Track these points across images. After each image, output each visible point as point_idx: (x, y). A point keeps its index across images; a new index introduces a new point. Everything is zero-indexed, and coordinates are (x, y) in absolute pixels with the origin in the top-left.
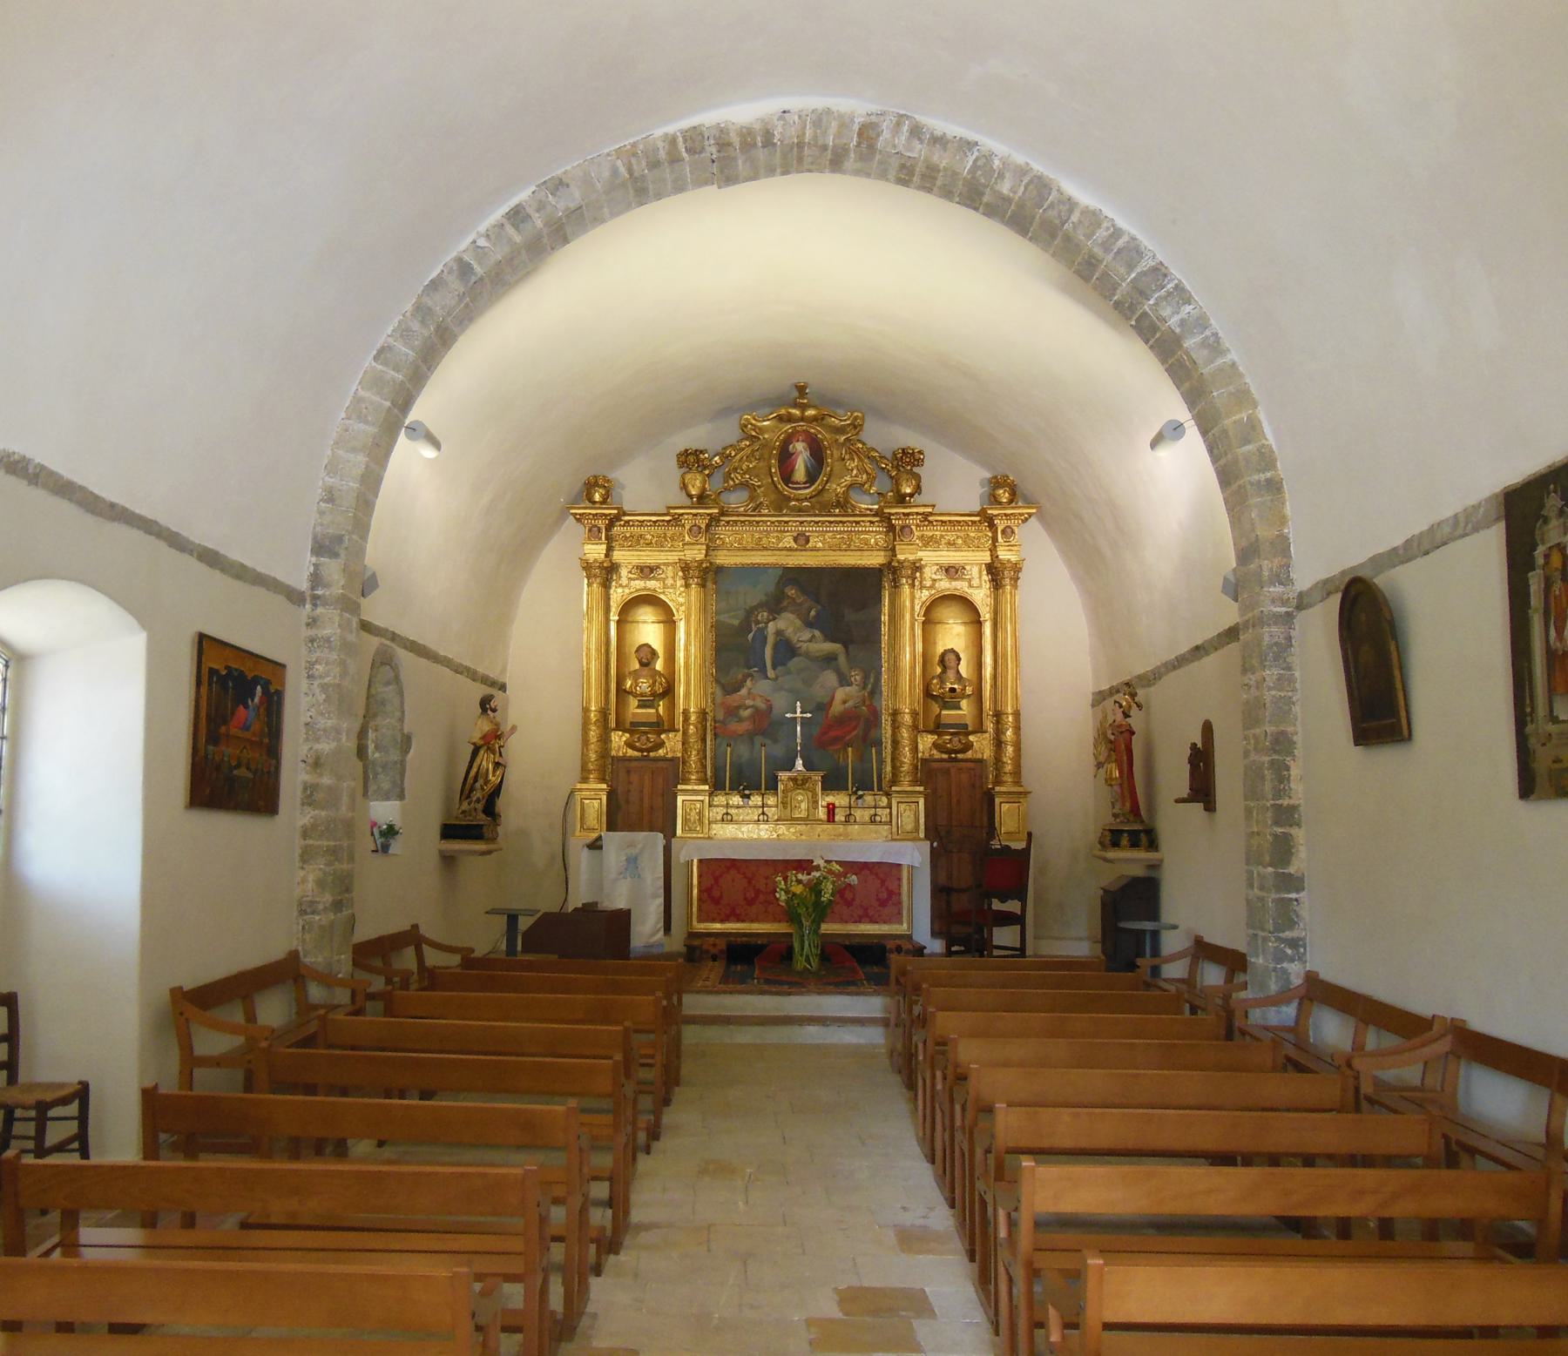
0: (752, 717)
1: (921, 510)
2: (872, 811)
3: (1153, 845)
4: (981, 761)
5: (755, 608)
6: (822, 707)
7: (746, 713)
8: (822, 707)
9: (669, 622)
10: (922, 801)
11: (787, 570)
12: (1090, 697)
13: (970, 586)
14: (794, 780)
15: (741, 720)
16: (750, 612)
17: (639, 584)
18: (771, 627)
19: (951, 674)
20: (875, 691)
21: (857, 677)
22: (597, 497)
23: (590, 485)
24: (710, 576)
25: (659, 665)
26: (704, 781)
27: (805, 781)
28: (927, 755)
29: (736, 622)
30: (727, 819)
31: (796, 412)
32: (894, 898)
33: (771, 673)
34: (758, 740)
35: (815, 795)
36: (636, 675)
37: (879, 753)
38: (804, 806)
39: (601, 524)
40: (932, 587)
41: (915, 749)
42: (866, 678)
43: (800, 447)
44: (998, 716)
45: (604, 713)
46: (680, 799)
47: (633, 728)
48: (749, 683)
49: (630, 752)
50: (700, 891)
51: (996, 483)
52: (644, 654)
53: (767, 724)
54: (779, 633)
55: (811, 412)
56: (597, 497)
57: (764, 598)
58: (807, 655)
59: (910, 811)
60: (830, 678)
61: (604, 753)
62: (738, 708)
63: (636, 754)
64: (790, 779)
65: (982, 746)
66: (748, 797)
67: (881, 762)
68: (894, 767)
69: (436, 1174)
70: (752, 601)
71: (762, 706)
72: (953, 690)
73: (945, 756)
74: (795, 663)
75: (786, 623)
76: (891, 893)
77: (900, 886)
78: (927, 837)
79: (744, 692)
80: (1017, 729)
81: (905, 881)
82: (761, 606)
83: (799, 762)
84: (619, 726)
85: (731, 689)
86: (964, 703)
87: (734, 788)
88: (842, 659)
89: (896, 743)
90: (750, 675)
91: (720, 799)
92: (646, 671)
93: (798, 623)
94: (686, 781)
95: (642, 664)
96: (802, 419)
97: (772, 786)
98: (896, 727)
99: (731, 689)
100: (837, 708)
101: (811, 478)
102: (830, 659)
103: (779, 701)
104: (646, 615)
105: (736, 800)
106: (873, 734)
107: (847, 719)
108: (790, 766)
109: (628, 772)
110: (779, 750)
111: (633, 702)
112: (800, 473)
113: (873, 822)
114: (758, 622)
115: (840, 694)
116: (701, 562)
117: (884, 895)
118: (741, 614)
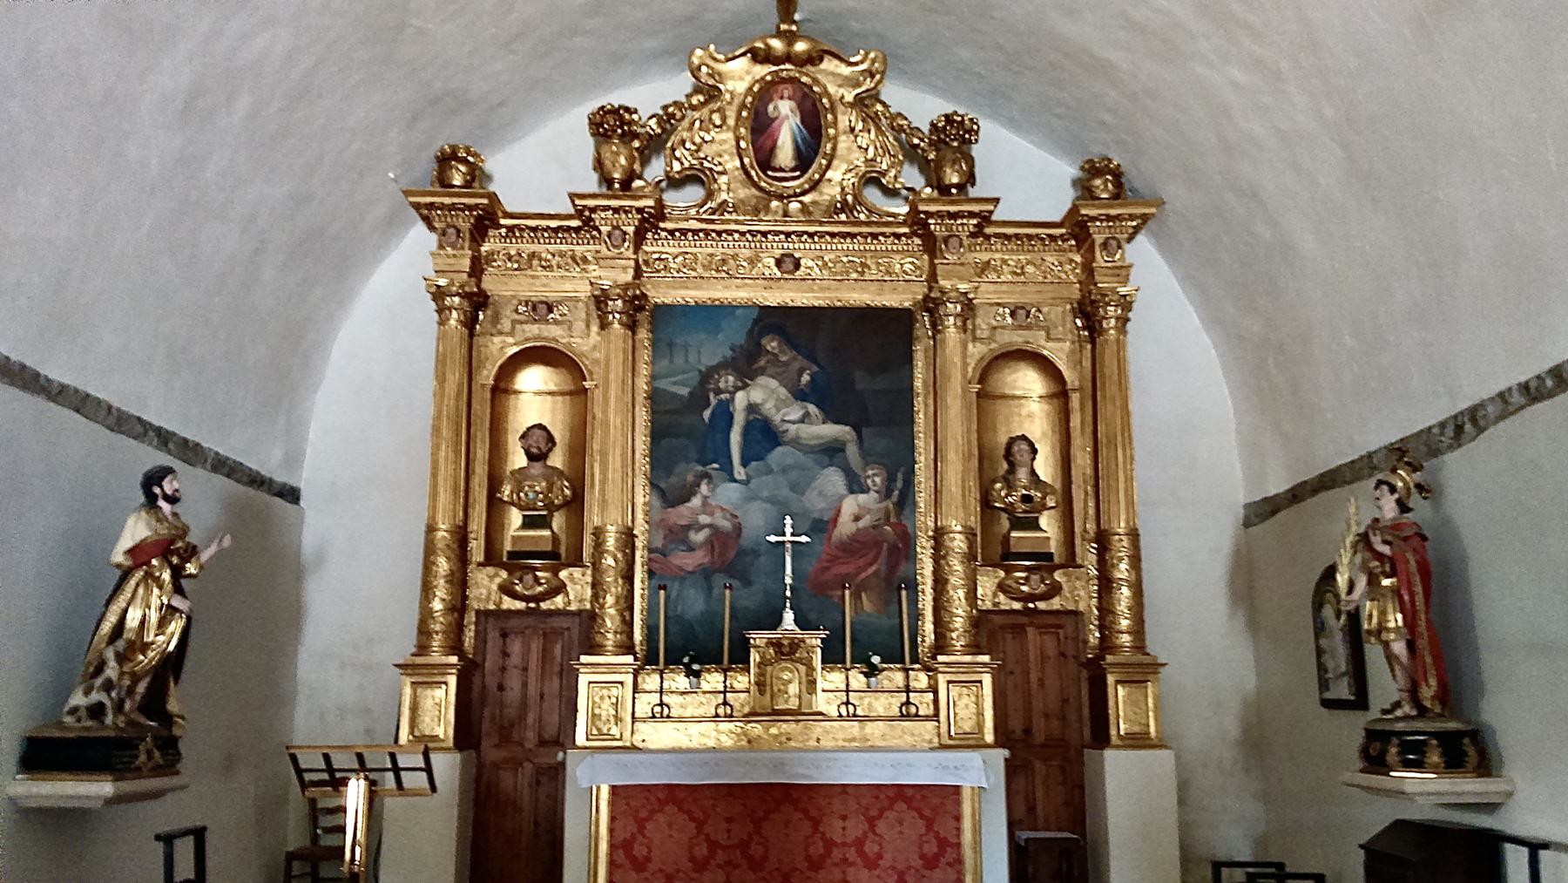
0: (710, 543)
1: (975, 208)
3: (1486, 766)
4: (1075, 613)
6: (821, 527)
7: (698, 537)
8: (821, 527)
9: (578, 394)
10: (987, 679)
12: (1241, 512)
13: (1049, 339)
14: (776, 645)
15: (691, 549)
16: (707, 376)
17: (533, 329)
18: (741, 399)
19: (1022, 475)
20: (906, 500)
21: (875, 479)
22: (457, 180)
23: (446, 160)
24: (642, 317)
25: (557, 460)
26: (628, 648)
27: (795, 645)
28: (988, 605)
29: (684, 391)
30: (661, 714)
31: (777, 44)
32: (950, 854)
33: (739, 472)
34: (719, 580)
35: (811, 669)
36: (520, 476)
37: (914, 601)
38: (793, 689)
39: (465, 223)
40: (991, 339)
41: (972, 595)
42: (890, 480)
43: (785, 110)
44: (1103, 540)
45: (461, 536)
46: (583, 680)
47: (517, 562)
48: (704, 488)
49: (509, 603)
50: (612, 847)
51: (1093, 169)
52: (538, 439)
53: (733, 556)
54: (752, 408)
55: (801, 46)
56: (457, 180)
57: (729, 353)
58: (795, 442)
59: (971, 702)
60: (833, 480)
61: (458, 606)
62: (688, 528)
63: (520, 605)
64: (770, 643)
65: (1078, 593)
66: (697, 674)
67: (916, 616)
68: (938, 622)
69: (852, 623)
70: (710, 359)
71: (726, 525)
72: (1027, 499)
73: (1017, 606)
74: (778, 455)
76: (943, 844)
77: (959, 829)
78: (999, 743)
79: (696, 502)
80: (1136, 561)
81: (967, 824)
82: (725, 366)
83: (789, 616)
84: (491, 559)
86: (1044, 521)
87: (673, 660)
88: (852, 451)
89: (940, 582)
90: (707, 476)
91: (651, 681)
92: (537, 468)
93: (783, 391)
94: (595, 648)
95: (531, 457)
96: (788, 58)
97: (740, 658)
98: (939, 555)
100: (845, 527)
101: (804, 160)
102: (832, 452)
103: (755, 519)
104: (533, 379)
105: (680, 681)
106: (903, 569)
107: (857, 546)
108: (776, 622)
109: (504, 635)
110: (751, 599)
111: (515, 517)
112: (785, 155)
113: (905, 717)
114: (718, 392)
115: (850, 505)
116: (626, 287)
117: (931, 848)
118: (693, 378)
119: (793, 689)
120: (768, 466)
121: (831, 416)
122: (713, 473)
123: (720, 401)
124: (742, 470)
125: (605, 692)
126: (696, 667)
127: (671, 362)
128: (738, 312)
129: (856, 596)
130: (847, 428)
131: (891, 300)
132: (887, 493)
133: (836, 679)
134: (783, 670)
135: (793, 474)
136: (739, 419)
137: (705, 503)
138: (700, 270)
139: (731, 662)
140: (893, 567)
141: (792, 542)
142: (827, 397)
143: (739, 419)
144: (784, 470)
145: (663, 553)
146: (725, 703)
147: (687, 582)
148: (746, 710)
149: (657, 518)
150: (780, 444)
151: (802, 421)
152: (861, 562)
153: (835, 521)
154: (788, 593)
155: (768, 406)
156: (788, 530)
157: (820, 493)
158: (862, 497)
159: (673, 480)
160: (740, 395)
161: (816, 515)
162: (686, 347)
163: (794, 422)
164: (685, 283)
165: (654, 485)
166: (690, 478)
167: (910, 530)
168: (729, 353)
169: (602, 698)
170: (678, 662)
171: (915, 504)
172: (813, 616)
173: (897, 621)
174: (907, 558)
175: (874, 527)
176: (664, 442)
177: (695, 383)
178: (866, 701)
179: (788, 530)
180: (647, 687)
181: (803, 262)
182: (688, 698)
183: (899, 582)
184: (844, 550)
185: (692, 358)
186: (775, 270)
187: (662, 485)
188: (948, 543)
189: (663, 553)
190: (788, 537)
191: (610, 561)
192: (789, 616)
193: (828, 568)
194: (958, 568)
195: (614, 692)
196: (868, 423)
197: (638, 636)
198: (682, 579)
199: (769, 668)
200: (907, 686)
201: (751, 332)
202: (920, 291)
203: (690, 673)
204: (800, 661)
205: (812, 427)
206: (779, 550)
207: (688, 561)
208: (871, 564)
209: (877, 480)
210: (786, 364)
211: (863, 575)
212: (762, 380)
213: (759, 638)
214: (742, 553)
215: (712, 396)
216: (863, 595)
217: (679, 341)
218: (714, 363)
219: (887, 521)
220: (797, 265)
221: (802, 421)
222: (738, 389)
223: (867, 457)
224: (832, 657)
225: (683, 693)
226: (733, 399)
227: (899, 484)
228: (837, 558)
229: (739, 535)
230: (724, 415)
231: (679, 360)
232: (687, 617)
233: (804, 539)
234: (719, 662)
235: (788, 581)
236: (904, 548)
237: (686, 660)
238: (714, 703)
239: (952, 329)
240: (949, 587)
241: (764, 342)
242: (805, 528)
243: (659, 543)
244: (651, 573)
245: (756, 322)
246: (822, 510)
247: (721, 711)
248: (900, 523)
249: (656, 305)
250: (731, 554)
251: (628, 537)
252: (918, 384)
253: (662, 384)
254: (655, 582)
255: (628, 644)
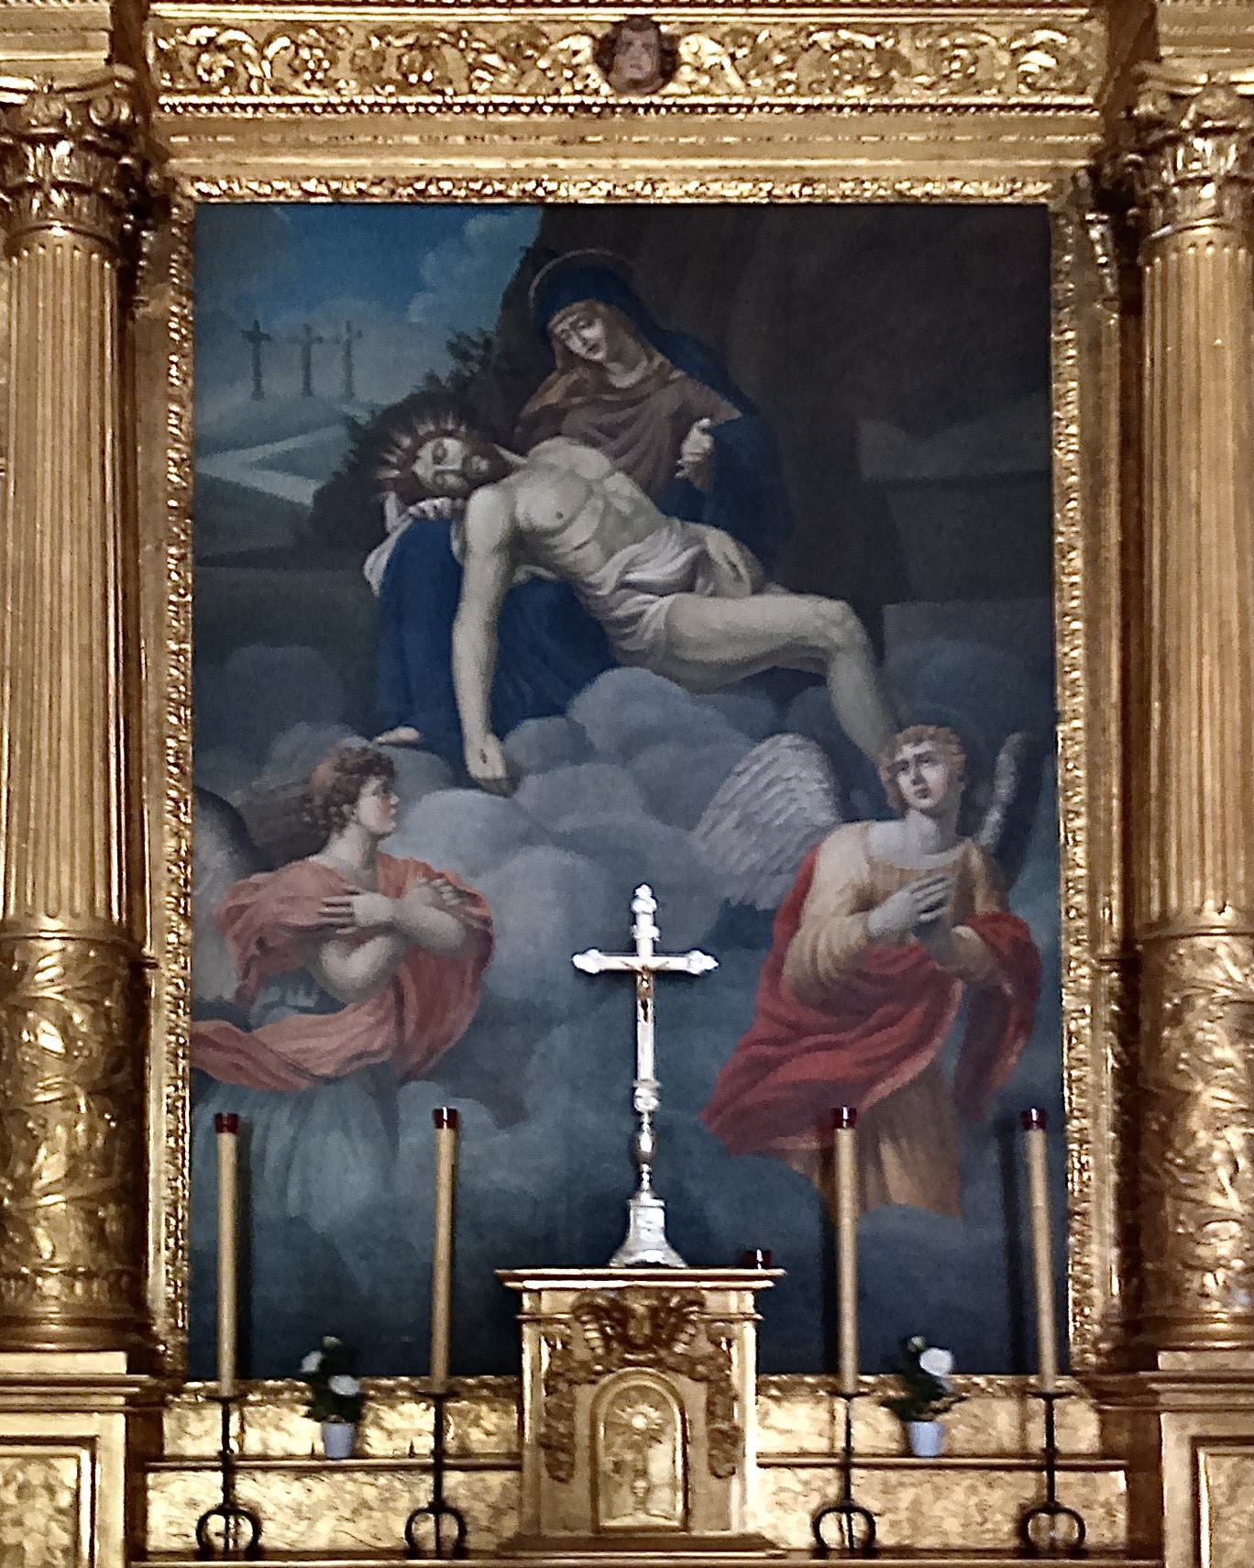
0: (389, 983)
2: (1027, 1486)
5: (400, 416)
6: (750, 929)
8: (750, 930)
11: (565, 220)
14: (612, 1314)
15: (329, 1002)
16: (375, 441)
20: (1024, 839)
21: (924, 768)
26: (98, 1329)
27: (670, 1318)
29: (301, 491)
33: (484, 755)
34: (421, 1098)
35: (722, 1396)
38: (663, 1461)
42: (975, 773)
48: (369, 807)
54: (522, 544)
55: (1179, 1161)
57: (445, 367)
58: (667, 656)
60: (788, 774)
62: (319, 935)
64: (587, 1308)
66: (352, 1411)
69: (860, 1239)
71: (440, 924)
74: (603, 700)
75: (565, 495)
79: (344, 851)
83: (648, 1218)
85: (268, 838)
87: (262, 1363)
88: (850, 685)
90: (379, 766)
93: (622, 488)
99: (268, 838)
100: (828, 929)
102: (781, 688)
103: (528, 904)
105: (290, 1429)
106: (1015, 1066)
107: (874, 989)
108: (607, 1238)
114: (413, 491)
115: (844, 858)
118: (332, 443)
119: (663, 1461)
120: (577, 732)
121: (780, 565)
122: (401, 759)
123: (421, 520)
124: (492, 748)
125: (35, 1474)
126: (344, 1386)
127: (258, 394)
128: (475, 226)
129: (867, 1155)
130: (832, 609)
131: (980, 181)
132: (960, 818)
133: (784, 1423)
134: (625, 1398)
135: (657, 759)
136: (482, 580)
137: (373, 857)
138: (351, 90)
139: (455, 1368)
140: (980, 1062)
141: (660, 975)
142: (760, 506)
143: (482, 580)
144: (630, 746)
145: (238, 1014)
146: (439, 1506)
147: (321, 1112)
148: (510, 1526)
149: (217, 900)
150: (615, 665)
151: (686, 584)
152: (885, 1041)
153: (793, 910)
154: (646, 1143)
155: (580, 532)
156: (646, 932)
157: (745, 823)
158: (882, 834)
159: (269, 779)
160: (482, 500)
161: (735, 892)
162: (308, 342)
163: (661, 590)
164: (300, 128)
165: (206, 799)
166: (325, 773)
167: (1040, 939)
168: (445, 367)
169: (23, 1491)
170: (289, 1369)
171: (1055, 854)
172: (720, 1216)
173: (994, 1233)
174: (1025, 1026)
175: (922, 929)
176: (247, 657)
177: (336, 464)
178: (906, 1496)
179: (646, 932)
180: (190, 1448)
181: (685, 50)
182: (321, 1488)
183: (1002, 1122)
184: (825, 1006)
185: (327, 384)
186: (596, 79)
187: (236, 798)
188: (1189, 969)
189: (238, 1014)
190: (645, 959)
191: (50, 1039)
192: (648, 1218)
193: (769, 1065)
194: (1226, 1053)
195: (66, 1471)
196: (903, 594)
197: (161, 1284)
198: (304, 1104)
199: (585, 1394)
200: (439, 1451)
201: (513, 297)
202: (1075, 148)
203: (325, 1407)
204: (688, 1365)
205: (719, 606)
206: (620, 999)
207: (329, 1042)
208: (912, 1049)
209: (933, 775)
210: (633, 398)
211: (883, 1089)
212: (557, 452)
213: (551, 1293)
214: (491, 1017)
215: (391, 505)
216: (887, 1152)
217: (284, 322)
218: (396, 397)
219: (965, 913)
220: (668, 64)
221: (686, 584)
222: (475, 483)
223: (902, 705)
224: (798, 1349)
225: (301, 1472)
226: (460, 515)
227: (1004, 788)
228: (798, 1030)
229: (484, 958)
230: (433, 568)
231: (282, 385)
232: (320, 1223)
233: (699, 963)
234: (421, 1368)
235: (646, 1100)
236: (1028, 976)
237: (312, 1363)
238: (404, 1503)
239: (1205, 231)
240: (1195, 1122)
241: (560, 324)
242: (704, 922)
243: (225, 985)
244: (200, 1083)
245: (533, 258)
246: (755, 873)
247: (425, 1527)
248: (1003, 916)
249: (204, 205)
250: (460, 1018)
251: (118, 965)
252: (1067, 453)
253: (228, 468)
254: (207, 1115)
255: (128, 1312)
